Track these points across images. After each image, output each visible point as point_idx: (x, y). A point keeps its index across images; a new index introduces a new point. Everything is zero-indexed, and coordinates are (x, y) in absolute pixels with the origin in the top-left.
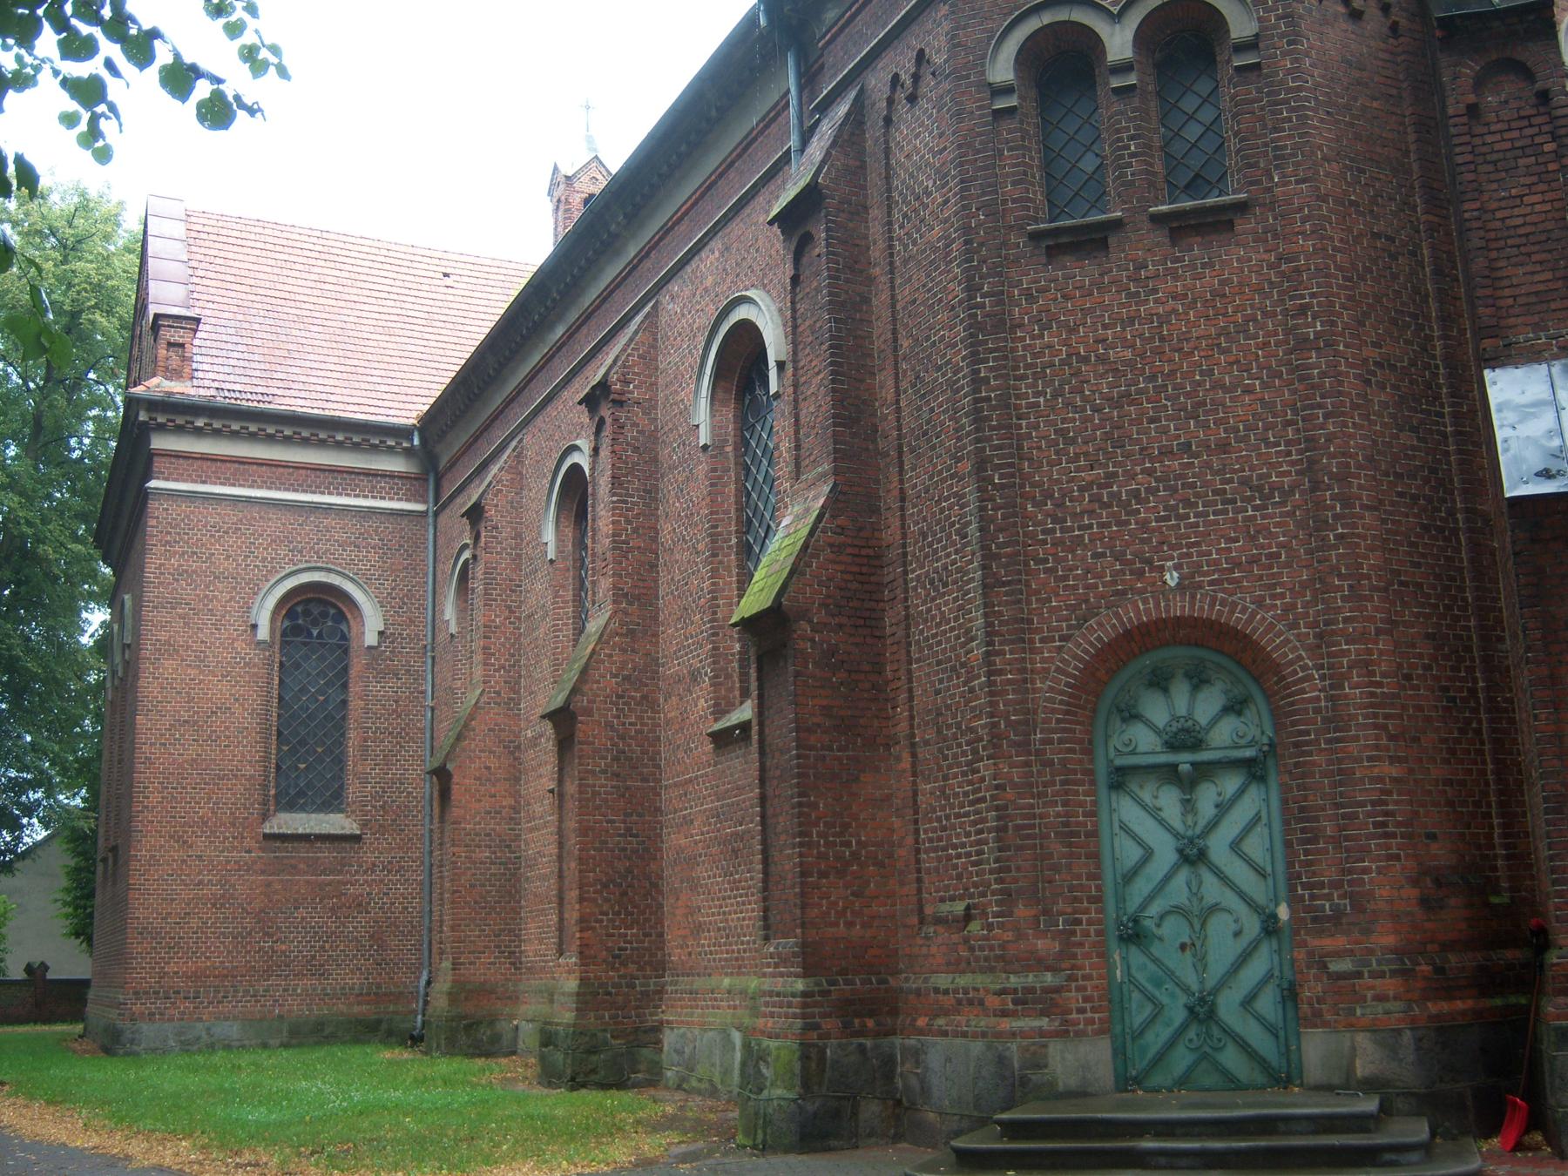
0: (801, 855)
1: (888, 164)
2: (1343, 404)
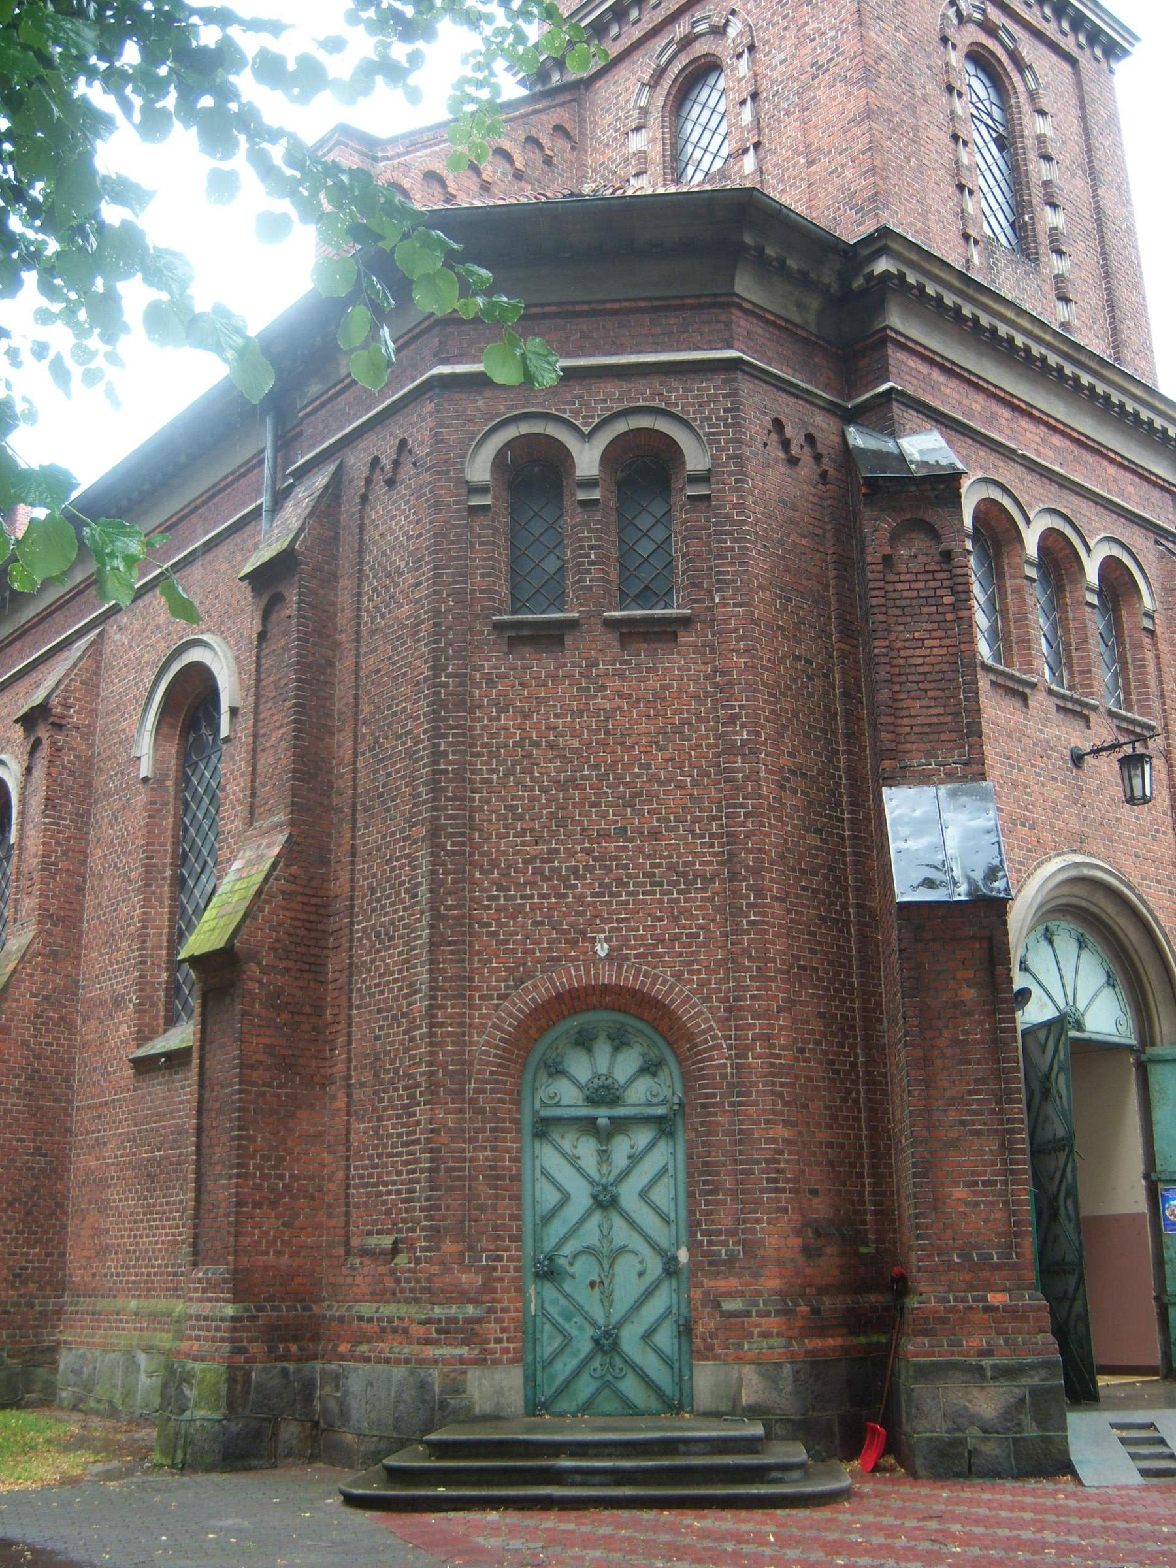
0: (237, 1186)
1: (361, 539)
2: (761, 806)
